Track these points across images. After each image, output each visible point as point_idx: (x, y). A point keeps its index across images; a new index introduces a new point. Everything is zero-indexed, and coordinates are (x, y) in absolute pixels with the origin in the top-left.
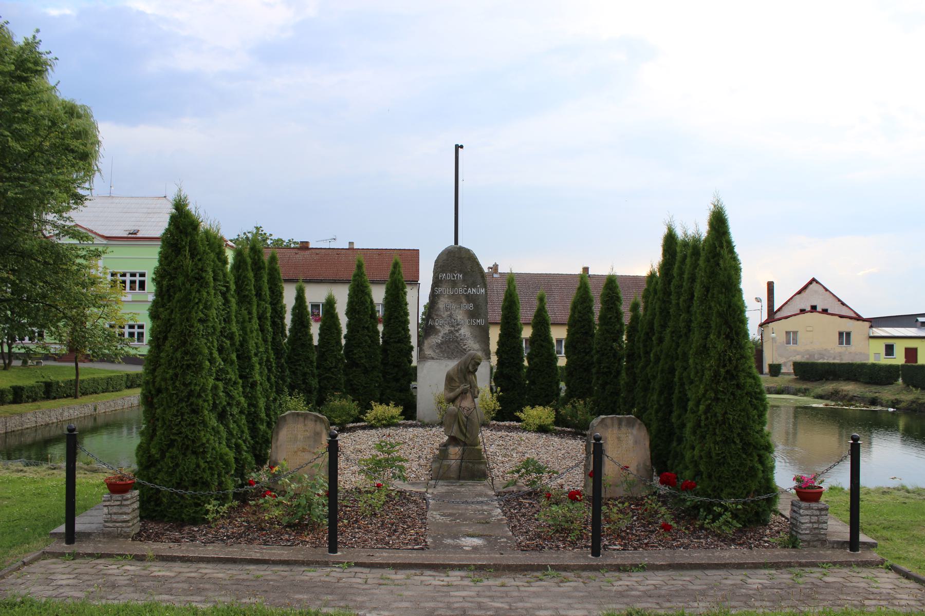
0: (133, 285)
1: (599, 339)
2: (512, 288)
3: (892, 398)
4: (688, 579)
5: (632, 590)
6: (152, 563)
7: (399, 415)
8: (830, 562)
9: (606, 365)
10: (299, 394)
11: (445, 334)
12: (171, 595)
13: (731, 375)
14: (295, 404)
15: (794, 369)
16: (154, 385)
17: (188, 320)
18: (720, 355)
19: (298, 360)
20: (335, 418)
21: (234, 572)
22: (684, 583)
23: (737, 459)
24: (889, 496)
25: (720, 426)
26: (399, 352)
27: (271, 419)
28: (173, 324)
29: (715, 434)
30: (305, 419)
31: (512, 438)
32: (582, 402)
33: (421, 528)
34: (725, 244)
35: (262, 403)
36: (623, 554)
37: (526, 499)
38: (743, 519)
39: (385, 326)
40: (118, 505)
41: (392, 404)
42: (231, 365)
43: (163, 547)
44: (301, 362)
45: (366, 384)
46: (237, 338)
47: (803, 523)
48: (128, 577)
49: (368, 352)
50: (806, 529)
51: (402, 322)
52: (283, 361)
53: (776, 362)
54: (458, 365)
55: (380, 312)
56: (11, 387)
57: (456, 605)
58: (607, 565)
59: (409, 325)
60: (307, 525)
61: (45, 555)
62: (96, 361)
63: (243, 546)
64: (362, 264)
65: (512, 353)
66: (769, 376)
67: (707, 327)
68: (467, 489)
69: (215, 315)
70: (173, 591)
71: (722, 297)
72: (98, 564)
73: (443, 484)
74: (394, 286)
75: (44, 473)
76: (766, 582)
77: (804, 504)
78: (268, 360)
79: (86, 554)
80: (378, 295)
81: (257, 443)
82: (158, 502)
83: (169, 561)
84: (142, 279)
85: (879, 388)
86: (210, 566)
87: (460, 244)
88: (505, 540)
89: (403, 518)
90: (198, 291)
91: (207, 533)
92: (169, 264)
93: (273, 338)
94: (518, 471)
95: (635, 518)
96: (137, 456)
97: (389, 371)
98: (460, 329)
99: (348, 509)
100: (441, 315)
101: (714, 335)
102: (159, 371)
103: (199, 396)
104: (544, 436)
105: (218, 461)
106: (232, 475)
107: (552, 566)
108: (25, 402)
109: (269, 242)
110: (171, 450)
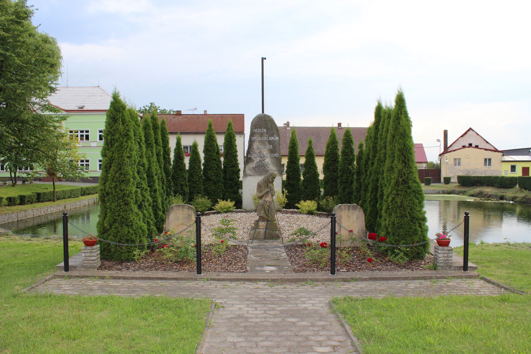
0: (82, 137)
1: (341, 164)
2: (294, 136)
3: (513, 195)
4: (379, 284)
5: (349, 289)
6: (109, 280)
7: (233, 206)
8: (452, 276)
9: (345, 178)
10: (179, 196)
11: (257, 162)
12: (120, 293)
13: (405, 182)
14: (177, 201)
15: (458, 180)
16: (105, 191)
17: (122, 157)
18: (399, 171)
19: (178, 178)
20: (199, 208)
21: (150, 283)
22: (376, 286)
23: (408, 225)
24: (498, 247)
25: (399, 208)
26: (232, 172)
27: (164, 209)
28: (114, 159)
29: (396, 212)
30: (183, 208)
31: (293, 218)
32: (331, 198)
33: (244, 262)
34: (403, 113)
35: (160, 200)
36: (347, 273)
37: (300, 248)
38: (411, 256)
39: (225, 158)
40: (90, 252)
41: (229, 200)
42: (144, 180)
43: (114, 273)
44: (180, 179)
45: (215, 190)
46: (147, 166)
47: (440, 257)
48: (98, 286)
49: (216, 173)
50: (441, 260)
51: (234, 156)
52: (170, 178)
53: (448, 176)
54: (264, 178)
55: (222, 150)
56: (18, 196)
57: (260, 296)
58: (338, 278)
59: (238, 158)
60: (185, 262)
61: (55, 277)
62: (64, 181)
63: (154, 271)
64: (211, 124)
65: (294, 172)
66: (443, 184)
67: (393, 157)
68: (269, 244)
69: (135, 154)
70: (121, 292)
71: (401, 141)
72: (82, 281)
73: (256, 241)
74: (229, 136)
75: (43, 241)
76: (418, 285)
77: (440, 248)
78: (162, 178)
79: (75, 276)
80: (220, 140)
81: (158, 221)
82: (109, 251)
83: (117, 279)
84: (87, 134)
85: (505, 190)
86: (138, 281)
87: (265, 113)
88: (287, 267)
89: (235, 258)
90: (126, 142)
91: (135, 266)
92: (111, 128)
93: (165, 166)
94: (296, 234)
95: (355, 257)
96: (97, 228)
97: (227, 182)
98: (265, 159)
99: (207, 254)
100: (255, 152)
101: (396, 161)
102: (108, 184)
103: (129, 196)
104: (311, 216)
105: (139, 229)
106: (146, 237)
107: (309, 279)
108: (27, 204)
109: (158, 111)
110: (115, 224)
